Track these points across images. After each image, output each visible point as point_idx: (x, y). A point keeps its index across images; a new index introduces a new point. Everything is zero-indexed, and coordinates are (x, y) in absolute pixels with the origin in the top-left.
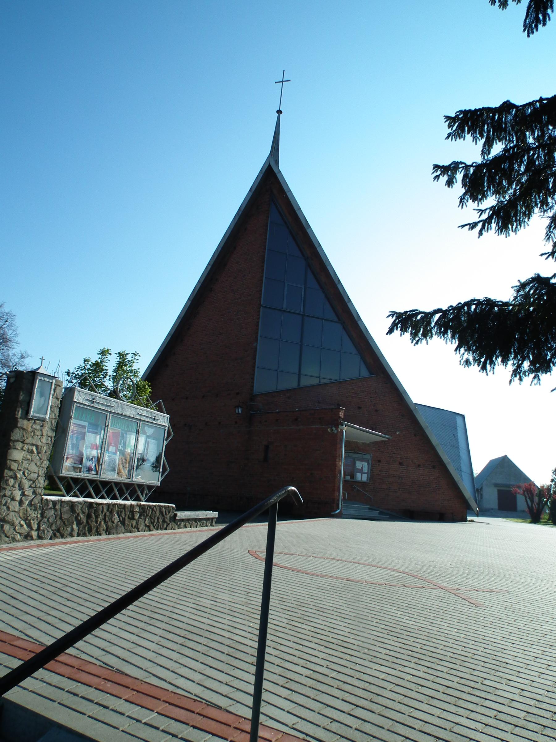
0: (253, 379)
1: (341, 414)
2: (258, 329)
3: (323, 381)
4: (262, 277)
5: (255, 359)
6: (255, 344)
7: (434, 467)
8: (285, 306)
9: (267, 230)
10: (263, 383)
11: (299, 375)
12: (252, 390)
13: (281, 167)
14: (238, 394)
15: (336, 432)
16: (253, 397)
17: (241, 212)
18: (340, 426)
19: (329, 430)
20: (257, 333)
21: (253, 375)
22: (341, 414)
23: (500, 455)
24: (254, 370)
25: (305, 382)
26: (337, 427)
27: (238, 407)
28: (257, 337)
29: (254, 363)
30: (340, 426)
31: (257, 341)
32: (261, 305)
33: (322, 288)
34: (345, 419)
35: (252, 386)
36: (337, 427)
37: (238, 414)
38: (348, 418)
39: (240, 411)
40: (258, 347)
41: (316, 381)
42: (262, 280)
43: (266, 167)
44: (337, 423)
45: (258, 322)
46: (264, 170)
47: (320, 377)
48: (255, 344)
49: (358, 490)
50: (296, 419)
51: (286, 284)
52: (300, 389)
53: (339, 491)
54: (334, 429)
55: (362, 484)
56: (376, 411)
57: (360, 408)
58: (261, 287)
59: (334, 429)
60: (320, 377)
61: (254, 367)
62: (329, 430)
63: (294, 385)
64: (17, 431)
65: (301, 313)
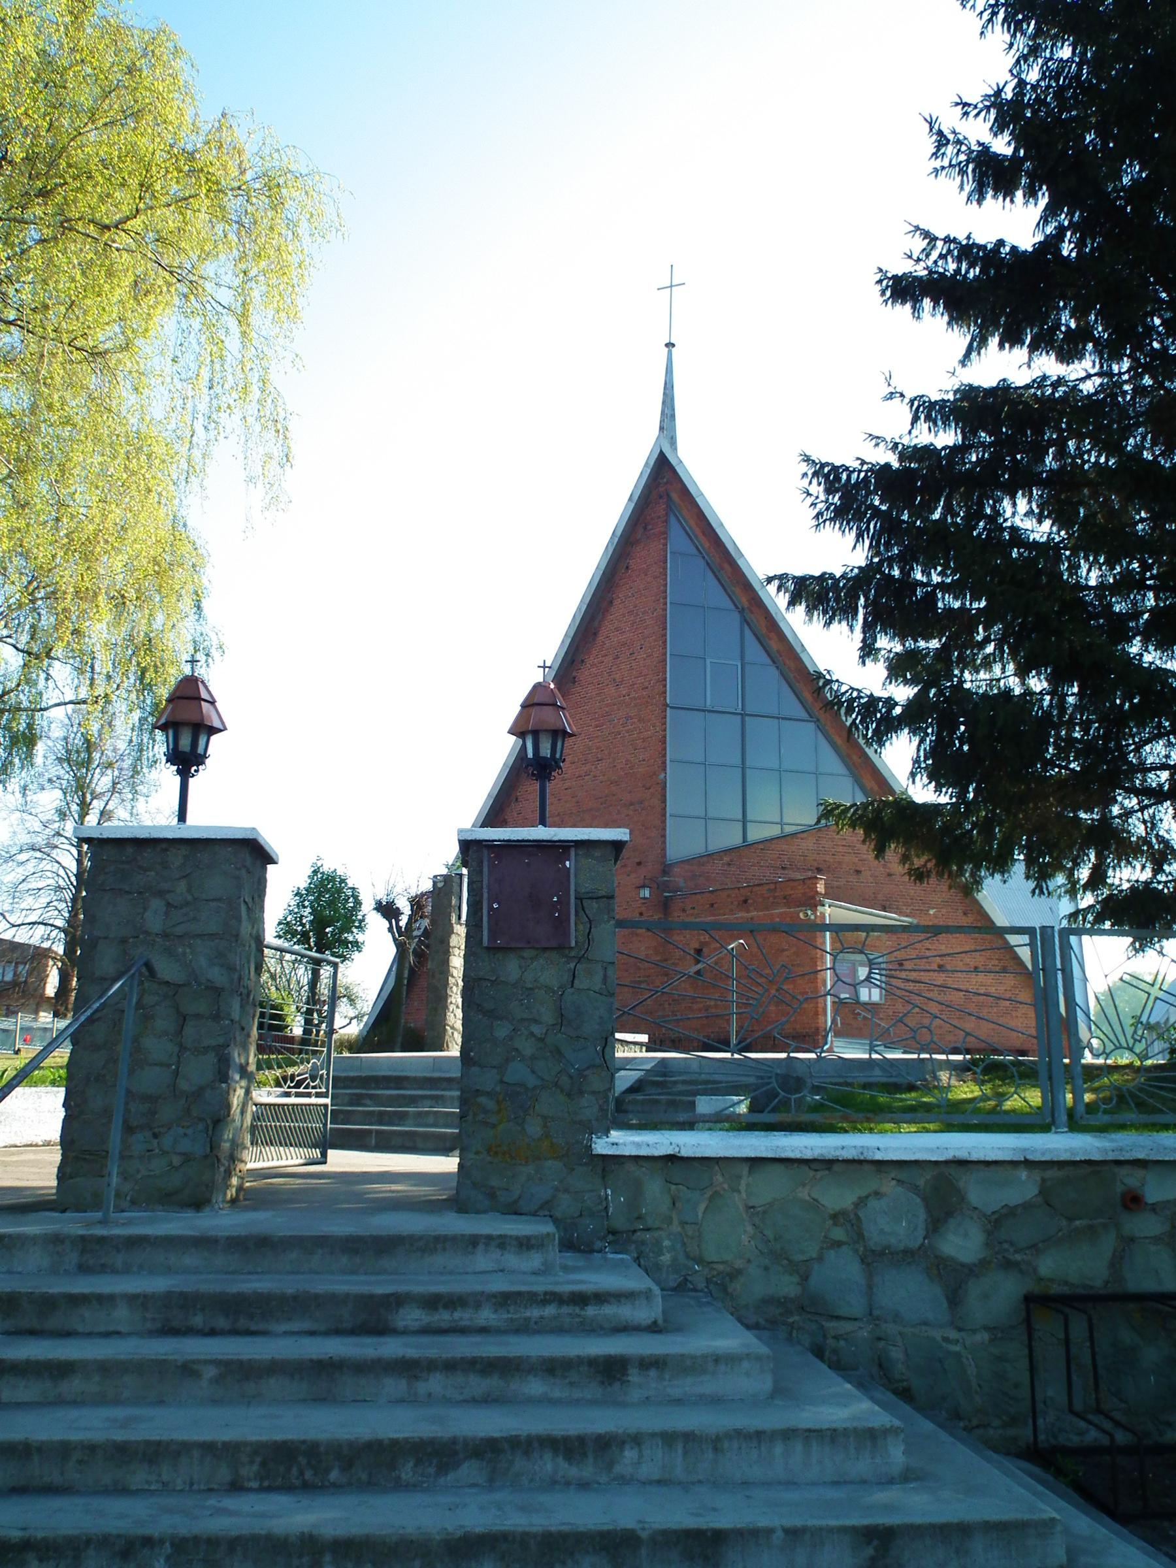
0: (664, 836)
1: (821, 888)
2: (665, 749)
3: (789, 829)
4: (665, 654)
5: (664, 801)
6: (662, 776)
7: (1004, 970)
8: (708, 703)
9: (665, 569)
10: (682, 842)
11: (744, 822)
12: (664, 856)
13: (681, 453)
14: (639, 864)
15: (813, 917)
16: (666, 869)
17: (616, 540)
18: (819, 908)
19: (802, 916)
20: (665, 755)
21: (664, 829)
22: (821, 888)
23: (280, 862)
24: (664, 822)
25: (756, 833)
26: (814, 908)
27: (644, 887)
28: (664, 763)
29: (665, 809)
30: (819, 908)
31: (665, 770)
32: (667, 705)
33: (774, 662)
34: (827, 895)
35: (664, 849)
36: (814, 911)
37: (645, 898)
38: (835, 894)
39: (646, 893)
40: (849, 1522)
41: (775, 831)
42: (665, 660)
43: (656, 456)
44: (813, 902)
45: (665, 737)
46: (652, 463)
47: (781, 824)
48: (662, 776)
49: (865, 1018)
50: (745, 901)
51: (708, 661)
52: (747, 846)
53: (826, 1015)
54: (809, 912)
55: (871, 1006)
56: (889, 875)
57: (858, 872)
58: (665, 672)
59: (809, 912)
60: (781, 824)
61: (664, 815)
62: (802, 916)
63: (737, 840)
64: (453, 936)
65: (739, 711)
